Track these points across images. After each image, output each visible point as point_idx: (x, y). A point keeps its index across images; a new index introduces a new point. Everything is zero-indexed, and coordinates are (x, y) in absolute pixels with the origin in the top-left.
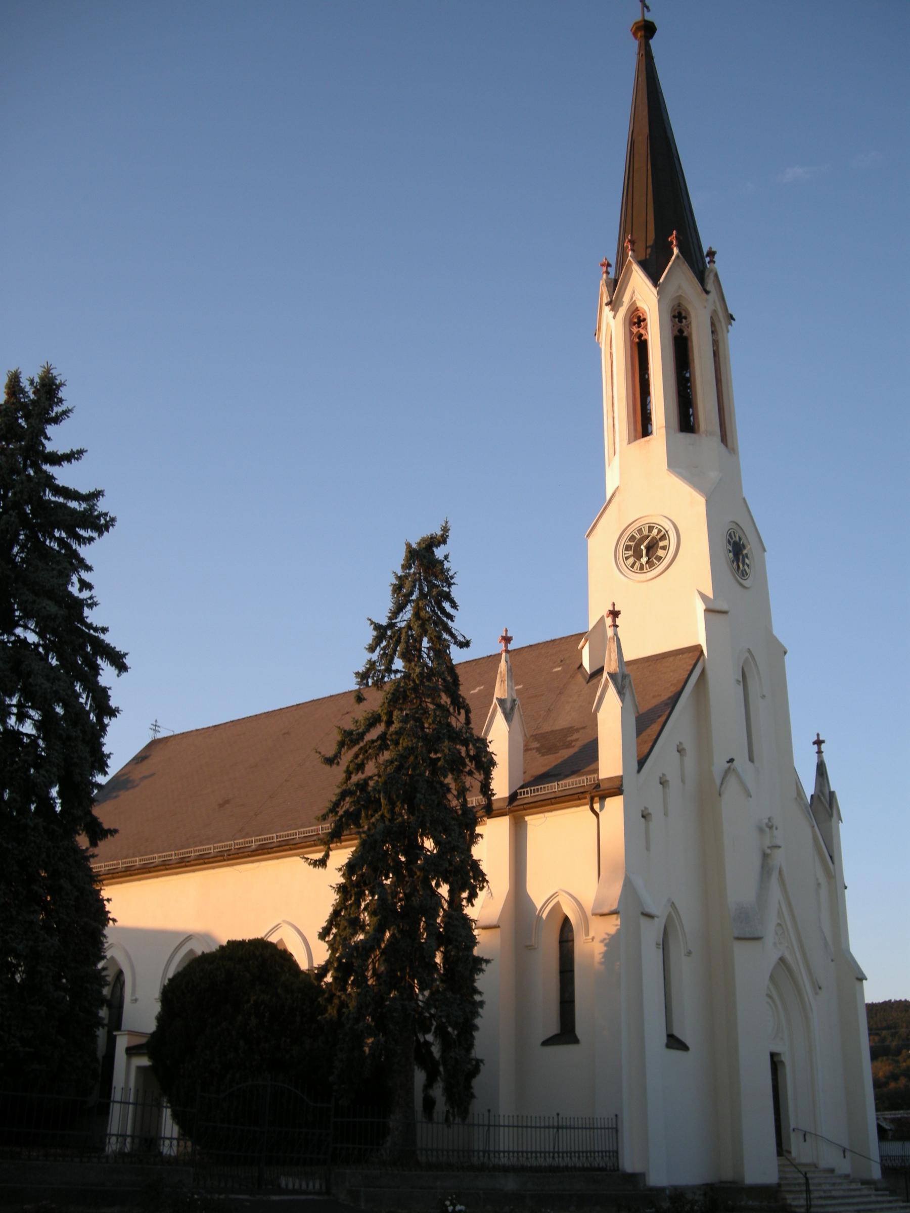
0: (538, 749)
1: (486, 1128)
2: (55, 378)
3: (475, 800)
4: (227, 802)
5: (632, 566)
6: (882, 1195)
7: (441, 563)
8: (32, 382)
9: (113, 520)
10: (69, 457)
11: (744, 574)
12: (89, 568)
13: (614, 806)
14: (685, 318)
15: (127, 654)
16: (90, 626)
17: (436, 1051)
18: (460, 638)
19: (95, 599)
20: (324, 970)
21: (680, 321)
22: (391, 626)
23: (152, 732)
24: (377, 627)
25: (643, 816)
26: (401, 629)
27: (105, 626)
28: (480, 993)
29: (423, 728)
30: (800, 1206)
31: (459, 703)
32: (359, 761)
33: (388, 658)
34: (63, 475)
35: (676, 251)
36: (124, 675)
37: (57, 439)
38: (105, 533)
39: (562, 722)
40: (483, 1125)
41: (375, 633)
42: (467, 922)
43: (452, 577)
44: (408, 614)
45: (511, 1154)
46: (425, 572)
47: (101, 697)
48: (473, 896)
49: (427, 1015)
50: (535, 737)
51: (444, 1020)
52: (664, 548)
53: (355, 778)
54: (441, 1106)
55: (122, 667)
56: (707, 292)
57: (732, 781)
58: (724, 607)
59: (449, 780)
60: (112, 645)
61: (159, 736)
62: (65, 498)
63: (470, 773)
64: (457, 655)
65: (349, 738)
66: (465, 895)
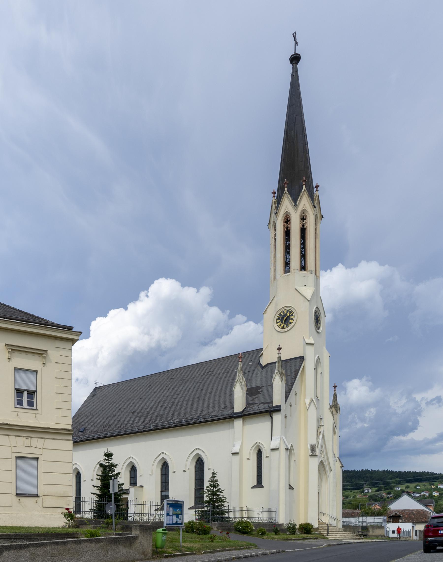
5: (280, 326)
13: (277, 417)
21: (303, 221)
52: (292, 319)
56: (315, 207)
57: (312, 404)
58: (312, 342)
61: (98, 386)
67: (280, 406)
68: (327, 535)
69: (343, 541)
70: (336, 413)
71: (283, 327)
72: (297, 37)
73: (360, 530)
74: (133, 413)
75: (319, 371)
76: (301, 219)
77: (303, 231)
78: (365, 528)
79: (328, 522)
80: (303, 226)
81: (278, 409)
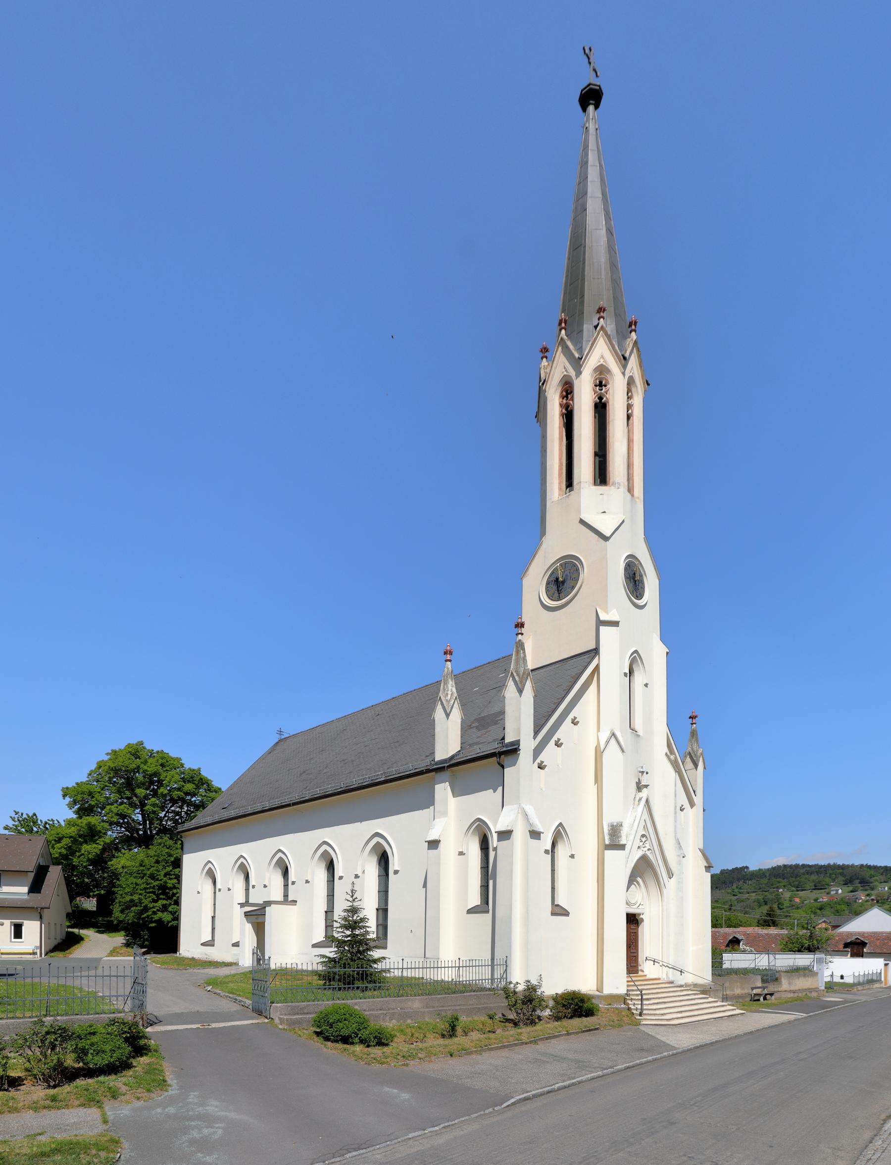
11: (639, 596)
61: (283, 737)
67: (517, 743)
68: (640, 1015)
73: (759, 984)
76: (596, 386)
77: (601, 408)
79: (665, 976)
80: (600, 398)
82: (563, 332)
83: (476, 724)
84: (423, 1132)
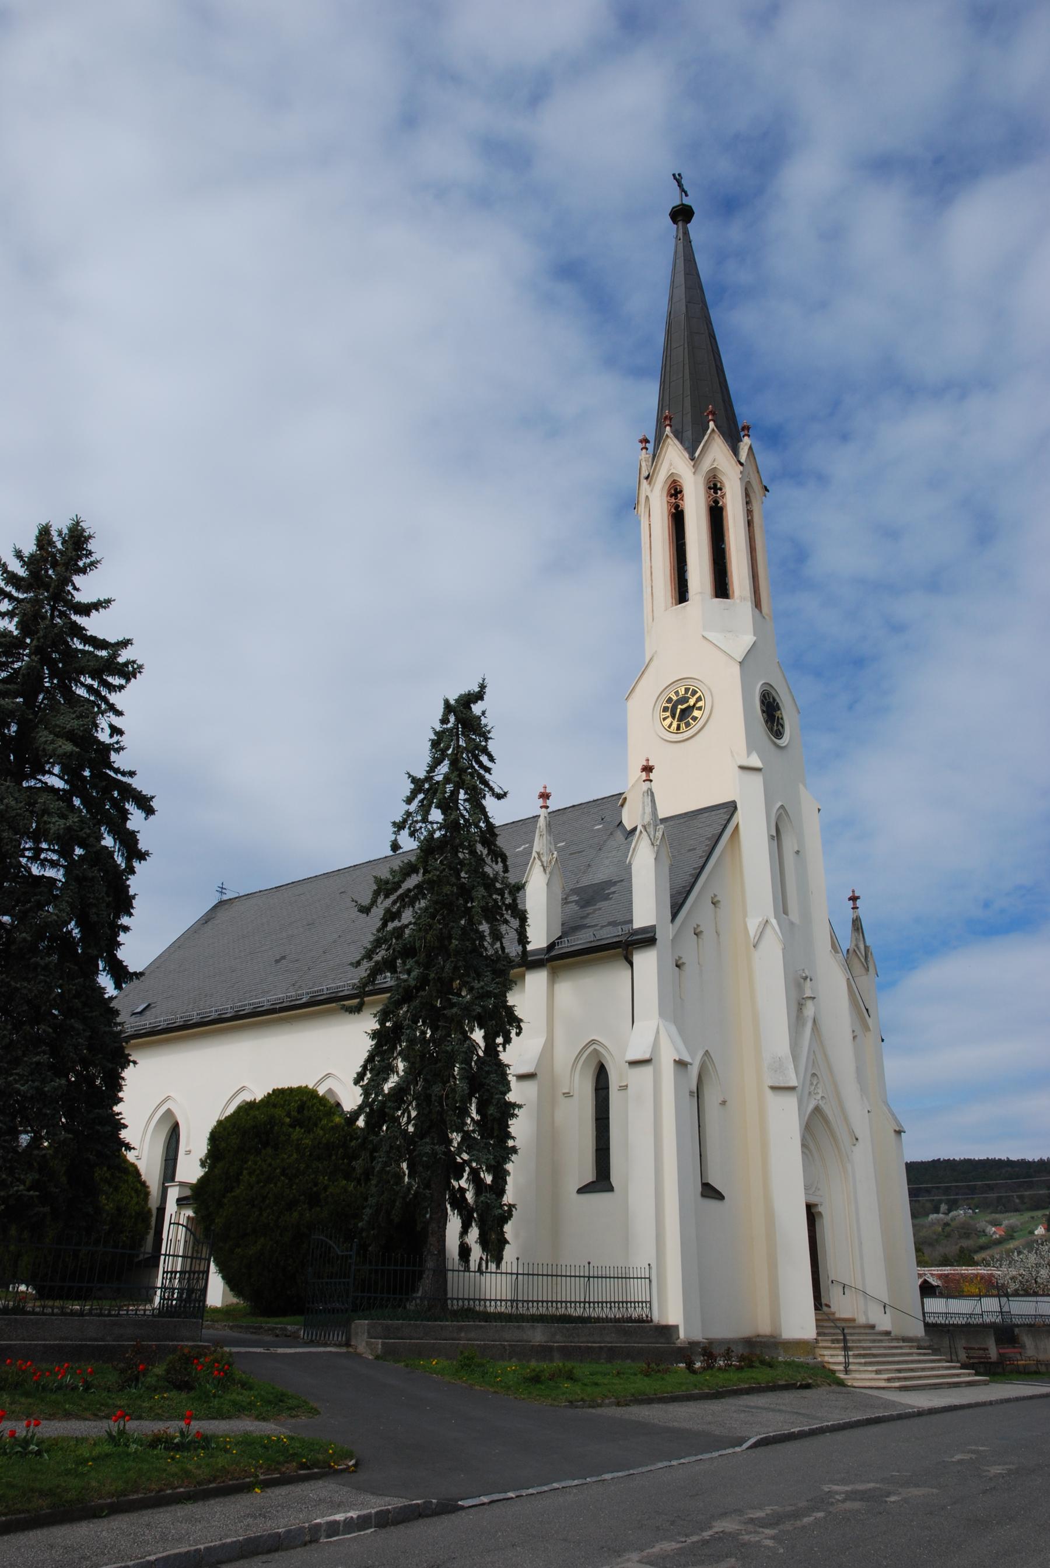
0: (576, 902)
1: (514, 1276)
2: (83, 530)
3: (513, 949)
4: (283, 958)
5: (670, 727)
6: (925, 1354)
7: (479, 718)
8: (60, 534)
9: (140, 667)
10: (97, 606)
11: (778, 734)
12: (119, 713)
13: (645, 961)
14: (721, 489)
15: (153, 797)
16: (117, 771)
17: (469, 1196)
18: (497, 790)
19: (122, 744)
20: (355, 1115)
22: (428, 779)
23: (218, 894)
24: (414, 780)
25: (677, 966)
26: (438, 782)
27: (133, 769)
28: (513, 1138)
29: (459, 878)
30: (839, 1363)
31: (499, 856)
32: (394, 909)
33: (424, 809)
34: (94, 625)
35: (712, 424)
36: (152, 818)
37: (86, 588)
38: (133, 680)
39: (600, 874)
40: (512, 1274)
41: (412, 786)
42: (501, 1069)
43: (489, 732)
44: (444, 768)
45: (499, 1303)
46: (463, 730)
47: (129, 843)
48: (507, 1040)
49: (459, 1160)
50: (574, 891)
51: (474, 1165)
52: (700, 709)
53: (391, 926)
54: (477, 1253)
55: (149, 811)
57: (769, 931)
58: (758, 764)
59: (485, 927)
60: (139, 789)
61: (225, 897)
62: (94, 648)
63: (506, 922)
64: (498, 812)
65: (384, 888)
66: (500, 1040)
69: (894, 1404)
70: (863, 971)
71: (678, 728)
72: (683, 182)
74: (277, 961)
75: (789, 844)
77: (716, 515)
78: (1006, 1333)
81: (647, 939)
82: (668, 428)
83: (575, 898)
84: (584, 1481)
